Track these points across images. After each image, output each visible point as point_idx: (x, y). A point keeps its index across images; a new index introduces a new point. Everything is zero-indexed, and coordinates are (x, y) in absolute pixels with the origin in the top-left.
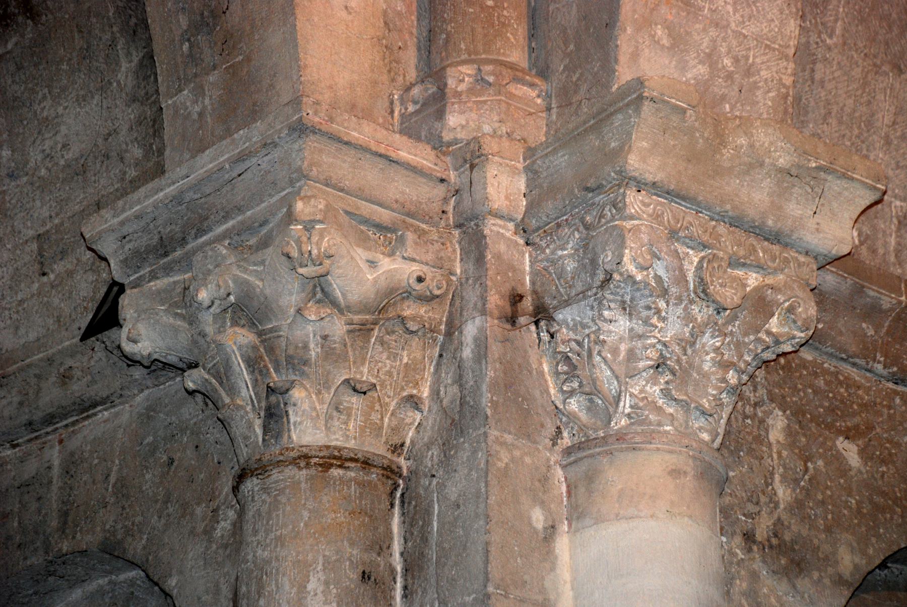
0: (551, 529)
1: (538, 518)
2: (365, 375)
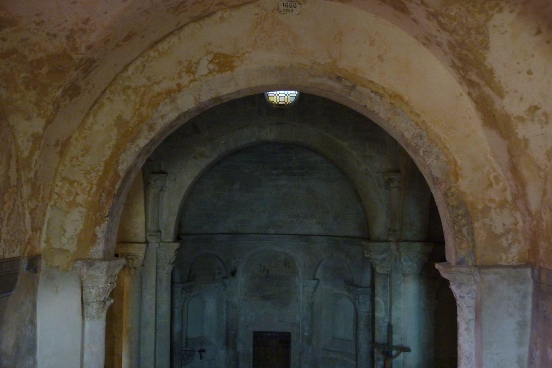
0: (401, 283)
1: (399, 282)
2: (383, 265)
